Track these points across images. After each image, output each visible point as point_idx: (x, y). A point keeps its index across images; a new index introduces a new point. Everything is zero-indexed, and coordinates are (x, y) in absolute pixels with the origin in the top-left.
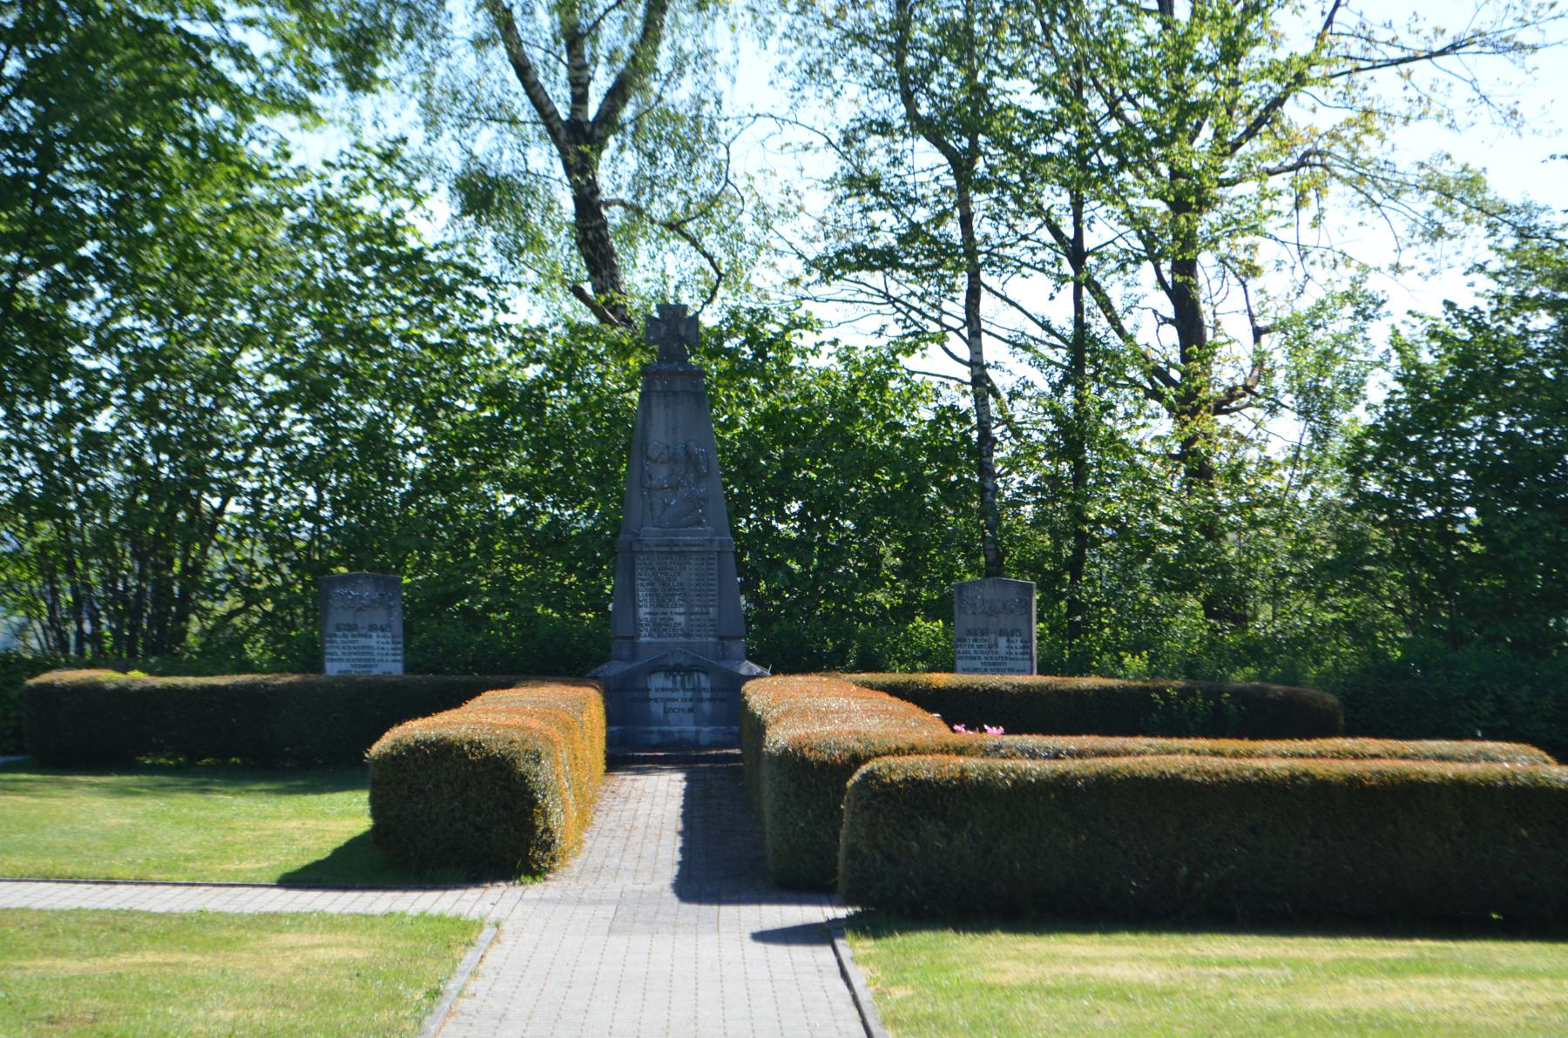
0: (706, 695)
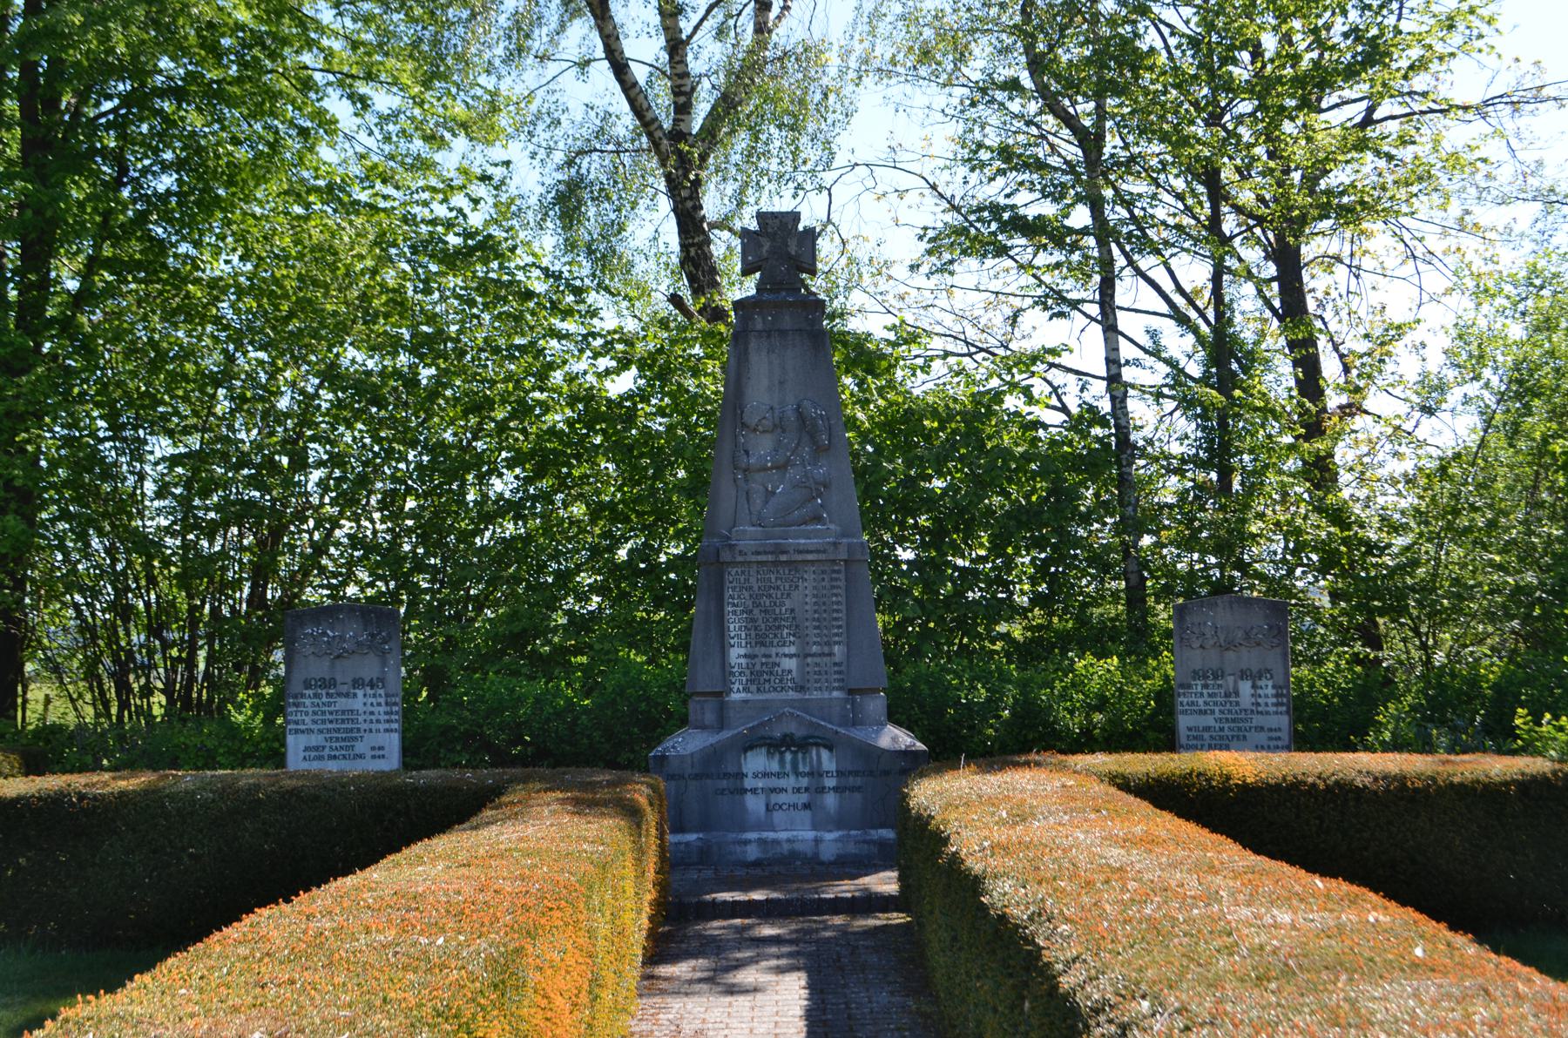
0: (830, 782)
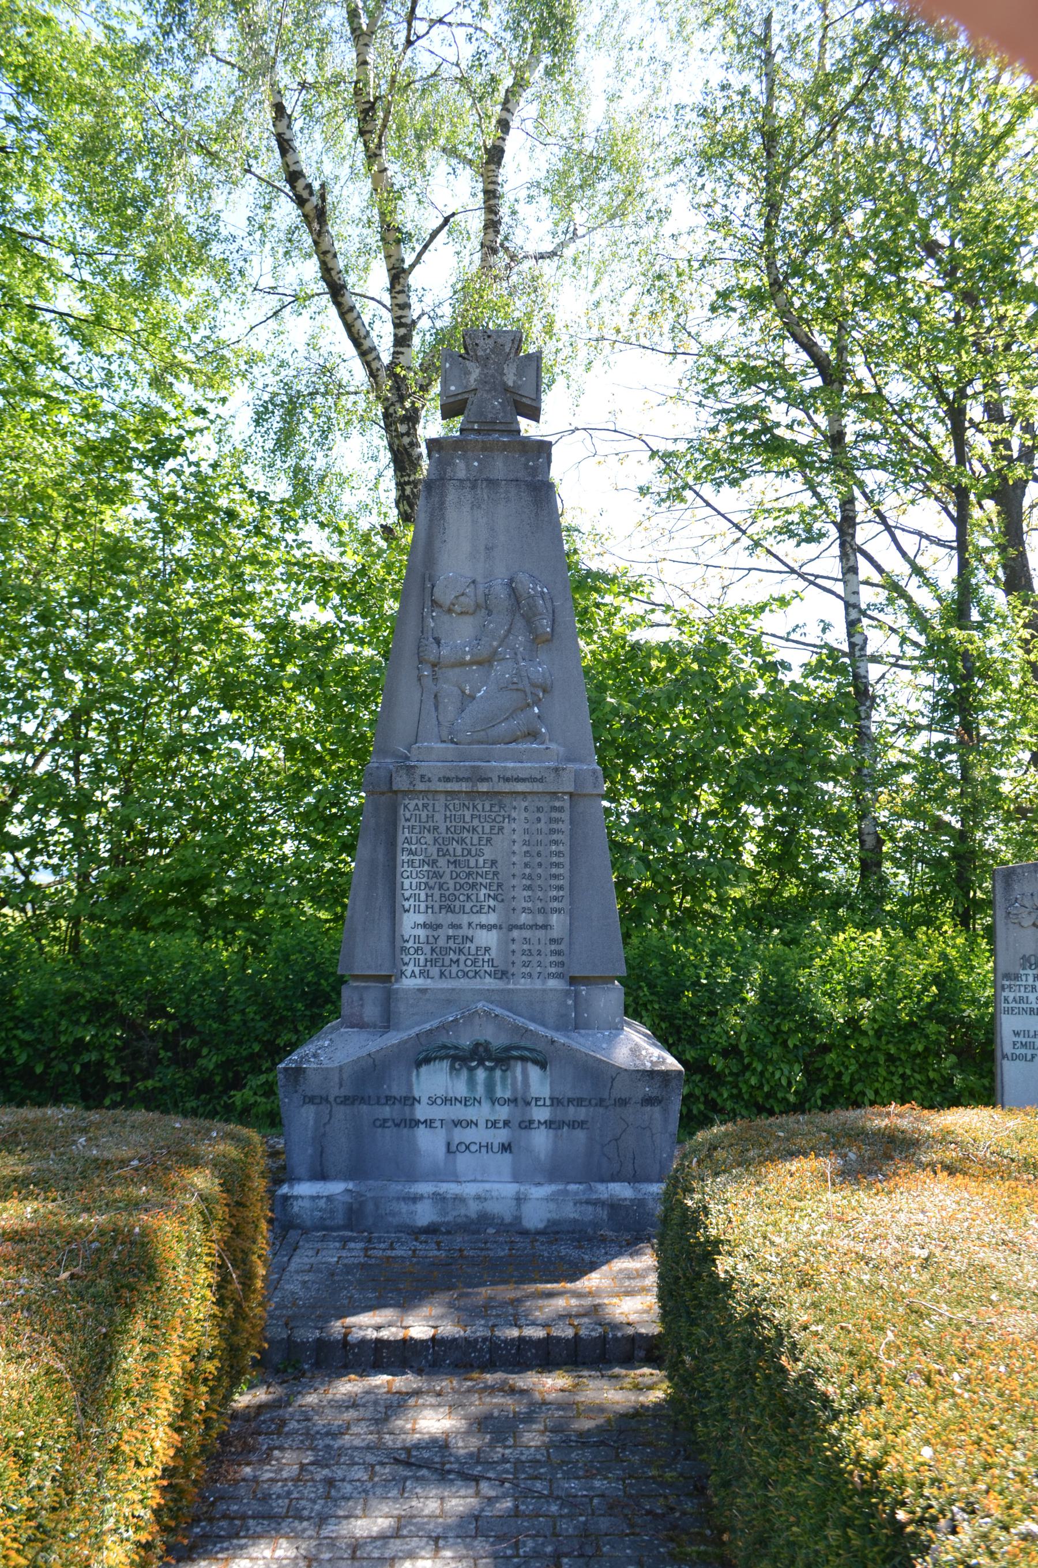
0: (541, 1114)
